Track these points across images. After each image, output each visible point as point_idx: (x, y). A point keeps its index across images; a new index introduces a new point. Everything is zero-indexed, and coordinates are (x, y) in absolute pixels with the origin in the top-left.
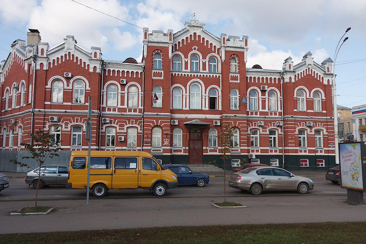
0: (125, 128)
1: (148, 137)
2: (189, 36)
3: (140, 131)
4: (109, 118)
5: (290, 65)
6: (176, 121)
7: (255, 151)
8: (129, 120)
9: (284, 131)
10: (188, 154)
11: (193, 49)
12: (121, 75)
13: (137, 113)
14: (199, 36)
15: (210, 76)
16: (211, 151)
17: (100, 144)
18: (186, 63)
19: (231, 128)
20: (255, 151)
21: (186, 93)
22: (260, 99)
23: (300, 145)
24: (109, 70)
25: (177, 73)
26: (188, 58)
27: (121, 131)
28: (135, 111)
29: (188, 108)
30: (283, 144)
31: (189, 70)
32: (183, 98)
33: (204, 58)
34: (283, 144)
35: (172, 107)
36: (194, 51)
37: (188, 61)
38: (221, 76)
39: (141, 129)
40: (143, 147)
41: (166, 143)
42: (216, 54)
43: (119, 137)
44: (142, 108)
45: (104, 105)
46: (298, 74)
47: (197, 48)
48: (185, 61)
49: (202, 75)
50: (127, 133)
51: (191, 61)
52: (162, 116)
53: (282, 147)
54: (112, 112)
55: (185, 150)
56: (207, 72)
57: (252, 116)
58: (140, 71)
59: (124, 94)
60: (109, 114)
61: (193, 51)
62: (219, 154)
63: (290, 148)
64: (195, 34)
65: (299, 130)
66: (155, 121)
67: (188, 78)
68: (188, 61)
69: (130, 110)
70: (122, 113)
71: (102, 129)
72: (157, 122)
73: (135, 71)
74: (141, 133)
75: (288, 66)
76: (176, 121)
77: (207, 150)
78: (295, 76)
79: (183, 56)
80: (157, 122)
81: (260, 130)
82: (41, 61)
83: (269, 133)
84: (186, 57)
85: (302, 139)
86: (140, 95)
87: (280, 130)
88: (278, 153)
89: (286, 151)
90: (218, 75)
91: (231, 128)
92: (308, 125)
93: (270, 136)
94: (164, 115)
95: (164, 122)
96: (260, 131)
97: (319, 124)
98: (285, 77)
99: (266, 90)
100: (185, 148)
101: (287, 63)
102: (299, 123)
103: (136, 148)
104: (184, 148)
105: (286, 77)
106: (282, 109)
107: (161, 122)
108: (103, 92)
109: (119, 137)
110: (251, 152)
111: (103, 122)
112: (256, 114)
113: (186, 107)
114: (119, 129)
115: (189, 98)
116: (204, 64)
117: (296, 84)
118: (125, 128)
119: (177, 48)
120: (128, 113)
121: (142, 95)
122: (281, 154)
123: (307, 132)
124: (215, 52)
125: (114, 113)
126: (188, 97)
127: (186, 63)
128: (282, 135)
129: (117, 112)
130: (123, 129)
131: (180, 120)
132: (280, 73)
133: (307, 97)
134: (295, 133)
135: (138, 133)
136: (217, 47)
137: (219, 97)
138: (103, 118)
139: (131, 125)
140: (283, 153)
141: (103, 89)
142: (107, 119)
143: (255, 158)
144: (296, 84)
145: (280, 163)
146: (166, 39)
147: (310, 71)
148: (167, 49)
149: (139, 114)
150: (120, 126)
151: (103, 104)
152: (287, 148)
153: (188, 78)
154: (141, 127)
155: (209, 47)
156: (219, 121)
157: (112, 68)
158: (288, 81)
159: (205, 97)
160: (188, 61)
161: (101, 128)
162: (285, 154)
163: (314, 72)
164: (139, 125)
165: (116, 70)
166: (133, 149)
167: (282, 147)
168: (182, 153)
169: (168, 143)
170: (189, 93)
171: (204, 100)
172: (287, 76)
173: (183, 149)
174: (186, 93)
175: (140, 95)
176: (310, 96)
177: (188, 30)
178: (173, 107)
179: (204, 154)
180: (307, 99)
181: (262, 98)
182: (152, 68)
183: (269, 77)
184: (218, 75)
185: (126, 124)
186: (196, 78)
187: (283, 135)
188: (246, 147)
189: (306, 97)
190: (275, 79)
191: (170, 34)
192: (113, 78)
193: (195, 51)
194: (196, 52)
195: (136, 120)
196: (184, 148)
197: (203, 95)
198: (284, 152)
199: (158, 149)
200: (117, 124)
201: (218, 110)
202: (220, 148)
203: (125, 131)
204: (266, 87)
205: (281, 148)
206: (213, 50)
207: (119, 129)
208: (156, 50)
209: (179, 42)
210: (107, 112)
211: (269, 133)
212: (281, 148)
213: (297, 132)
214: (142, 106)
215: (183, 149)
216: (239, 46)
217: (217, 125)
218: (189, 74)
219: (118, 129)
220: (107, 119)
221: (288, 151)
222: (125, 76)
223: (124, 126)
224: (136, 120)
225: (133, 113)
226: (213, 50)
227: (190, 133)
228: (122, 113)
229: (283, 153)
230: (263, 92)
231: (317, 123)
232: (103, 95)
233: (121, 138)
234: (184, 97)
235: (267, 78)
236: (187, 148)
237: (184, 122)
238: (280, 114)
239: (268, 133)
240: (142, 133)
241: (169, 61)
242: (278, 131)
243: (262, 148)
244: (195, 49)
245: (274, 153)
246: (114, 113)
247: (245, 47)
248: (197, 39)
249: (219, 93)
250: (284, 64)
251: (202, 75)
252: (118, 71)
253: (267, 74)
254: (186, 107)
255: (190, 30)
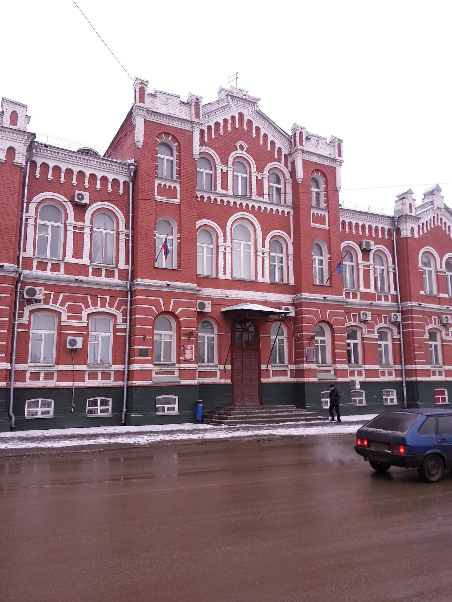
0: (84, 315)
1: (144, 339)
2: (228, 117)
3: (120, 325)
4: (43, 288)
5: (410, 204)
6: (206, 302)
7: (356, 372)
8: (94, 296)
9: (403, 332)
10: (229, 381)
11: (238, 146)
12: (75, 182)
13: (115, 280)
14: (250, 122)
15: (271, 209)
16: (276, 373)
17: (14, 357)
18: (225, 176)
19: (154, 320)
20: (356, 372)
21: (225, 241)
22: (361, 266)
23: (349, 362)
24: (45, 166)
25: (206, 195)
26: (229, 164)
27: (74, 324)
28: (110, 273)
29: (228, 277)
30: (403, 359)
31: (230, 192)
32: (217, 252)
33: (260, 169)
34: (403, 359)
35: (232, 274)
36: (239, 151)
37: (227, 171)
38: (292, 213)
39: (124, 321)
40: (129, 364)
41: (189, 354)
42: (283, 165)
43: (69, 338)
44: (129, 267)
45: (29, 253)
46: (423, 224)
47: (245, 146)
48: (222, 170)
49: (257, 205)
50: (86, 329)
51: (233, 173)
52: (180, 291)
53: (124, 364)
54: (48, 273)
55: (223, 372)
56: (265, 200)
57: (380, 302)
58: (122, 179)
59: (83, 229)
60: (94, 281)
61: (236, 152)
62: (292, 380)
63: (419, 367)
64: (241, 115)
65: (430, 331)
66: (161, 300)
67: (231, 210)
68: (227, 171)
69: (97, 272)
70: (77, 277)
71: (21, 315)
72: (167, 303)
73: (99, 175)
74: (124, 330)
75: (408, 206)
76: (206, 302)
77: (267, 371)
78: (419, 226)
79: (217, 160)
80: (167, 303)
81: (364, 330)
82: (14, 140)
83: (377, 337)
84: (260, 169)
85: (383, 349)
86: (123, 237)
87: (395, 330)
88: (393, 378)
89: (409, 373)
90: (286, 210)
91: (154, 320)
92: (393, 320)
93: (348, 341)
94: (183, 288)
95: (182, 305)
96: (362, 332)
97: (435, 319)
98: (402, 226)
99: (371, 248)
100: (223, 368)
101: (405, 201)
102: (428, 319)
103: (55, 369)
104: (222, 367)
105: (405, 228)
106: (398, 289)
107: (177, 305)
108: (26, 220)
109: (69, 338)
110: (31, 379)
111: (26, 296)
112: (355, 296)
113: (225, 273)
114: (69, 318)
115: (232, 253)
116: (260, 183)
117: (422, 242)
118: (84, 315)
119: (206, 140)
120: (91, 278)
121: (127, 236)
122: (399, 379)
123: (441, 335)
124: (279, 160)
125: (55, 274)
126: (228, 250)
127: (225, 176)
128: (400, 341)
129: (61, 274)
130: (80, 318)
131: (216, 302)
132: (390, 217)
133: (437, 268)
134: (425, 337)
135: (116, 330)
136: (285, 151)
137: (288, 256)
138: (26, 288)
139: (98, 309)
140: (404, 376)
141: (27, 211)
142: (37, 289)
143: (359, 389)
144: (422, 242)
145: (400, 397)
146: (184, 113)
147: (439, 221)
148: (189, 135)
149: (120, 282)
150: (71, 309)
151: (24, 250)
152: (413, 367)
153: (231, 210)
154: (124, 313)
155: (269, 149)
156: (209, 303)
157: (52, 161)
158: (409, 235)
159: (263, 254)
160: (229, 172)
161: (19, 313)
162: (408, 379)
163: (445, 223)
164: (118, 308)
165: (64, 167)
166: (103, 369)
167: (124, 364)
168: (216, 380)
169: (191, 356)
170: (232, 241)
171: (260, 260)
172: (406, 225)
173: (220, 370)
174: (225, 241)
175: (123, 237)
176: (441, 267)
177: (228, 106)
178: (233, 277)
179: (264, 380)
180: (437, 272)
181: (364, 266)
182: (155, 176)
183: (373, 225)
184: (286, 210)
185: (87, 307)
186: (244, 211)
187: (402, 340)
188: (345, 364)
189: (436, 267)
190: (383, 229)
191: (197, 104)
192: (55, 187)
193: (241, 152)
194: (243, 154)
195: (113, 298)
196: (222, 367)
197: (219, 244)
198: (405, 375)
199: (169, 368)
200: (62, 304)
201: (288, 285)
202: (293, 367)
203: (83, 323)
204: (372, 242)
205: (398, 367)
206: (276, 156)
207: (69, 318)
208: (172, 135)
209: (209, 128)
210: (35, 272)
211: (377, 337)
212: (398, 367)
213: (427, 336)
214: (127, 263)
215: (220, 370)
216: (326, 154)
217: (204, 311)
218: (232, 201)
219: (64, 317)
220: (37, 289)
221: (415, 373)
222: (87, 184)
223: (80, 310)
224: (113, 298)
225: (103, 279)
226: (276, 156)
227: (233, 331)
228: (77, 277)
229: (404, 376)
230: (366, 252)
231: (433, 317)
232: (26, 225)
233: (73, 342)
234: (221, 249)
235: (364, 226)
236: (229, 367)
237: (221, 306)
238: (395, 298)
239: (376, 335)
240: (128, 329)
241: (193, 164)
242: (392, 333)
243: (367, 367)
244: (241, 147)
245: (99, 383)
246: (55, 274)
247: (337, 158)
248: (245, 128)
249: (289, 248)
250: (396, 202)
251: (257, 205)
252: (69, 172)
253: (358, 216)
254: (225, 273)
255: (232, 104)
